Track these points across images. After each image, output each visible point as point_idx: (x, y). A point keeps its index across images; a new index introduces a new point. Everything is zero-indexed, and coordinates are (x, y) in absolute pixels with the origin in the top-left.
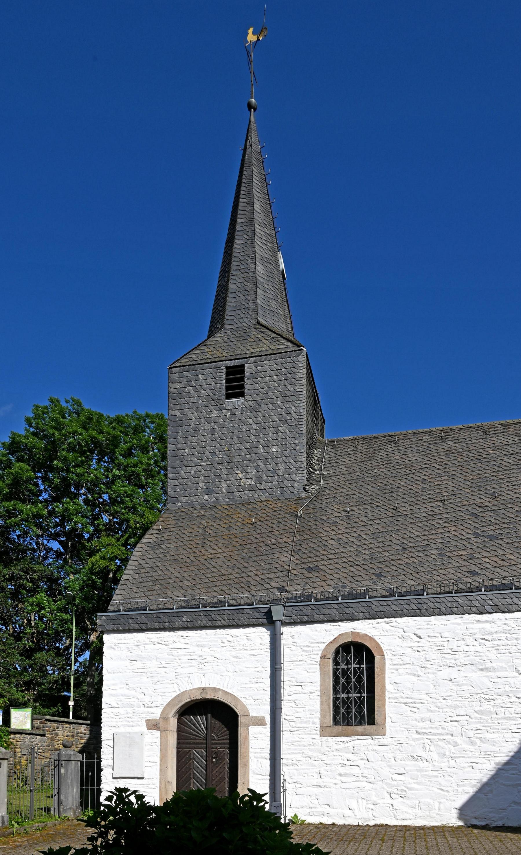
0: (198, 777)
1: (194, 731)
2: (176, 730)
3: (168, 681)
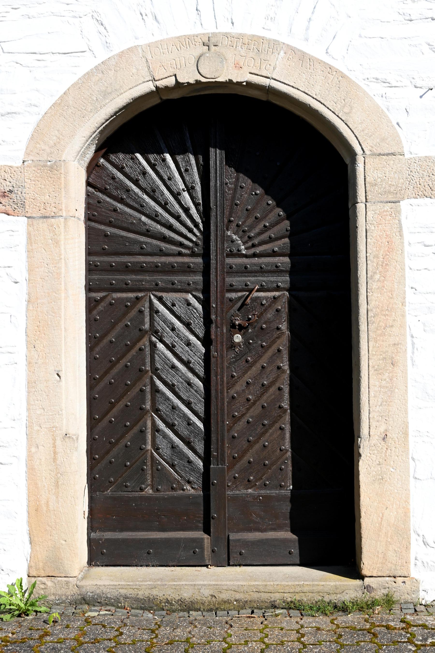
0: (174, 408)
1: (155, 217)
2: (82, 217)
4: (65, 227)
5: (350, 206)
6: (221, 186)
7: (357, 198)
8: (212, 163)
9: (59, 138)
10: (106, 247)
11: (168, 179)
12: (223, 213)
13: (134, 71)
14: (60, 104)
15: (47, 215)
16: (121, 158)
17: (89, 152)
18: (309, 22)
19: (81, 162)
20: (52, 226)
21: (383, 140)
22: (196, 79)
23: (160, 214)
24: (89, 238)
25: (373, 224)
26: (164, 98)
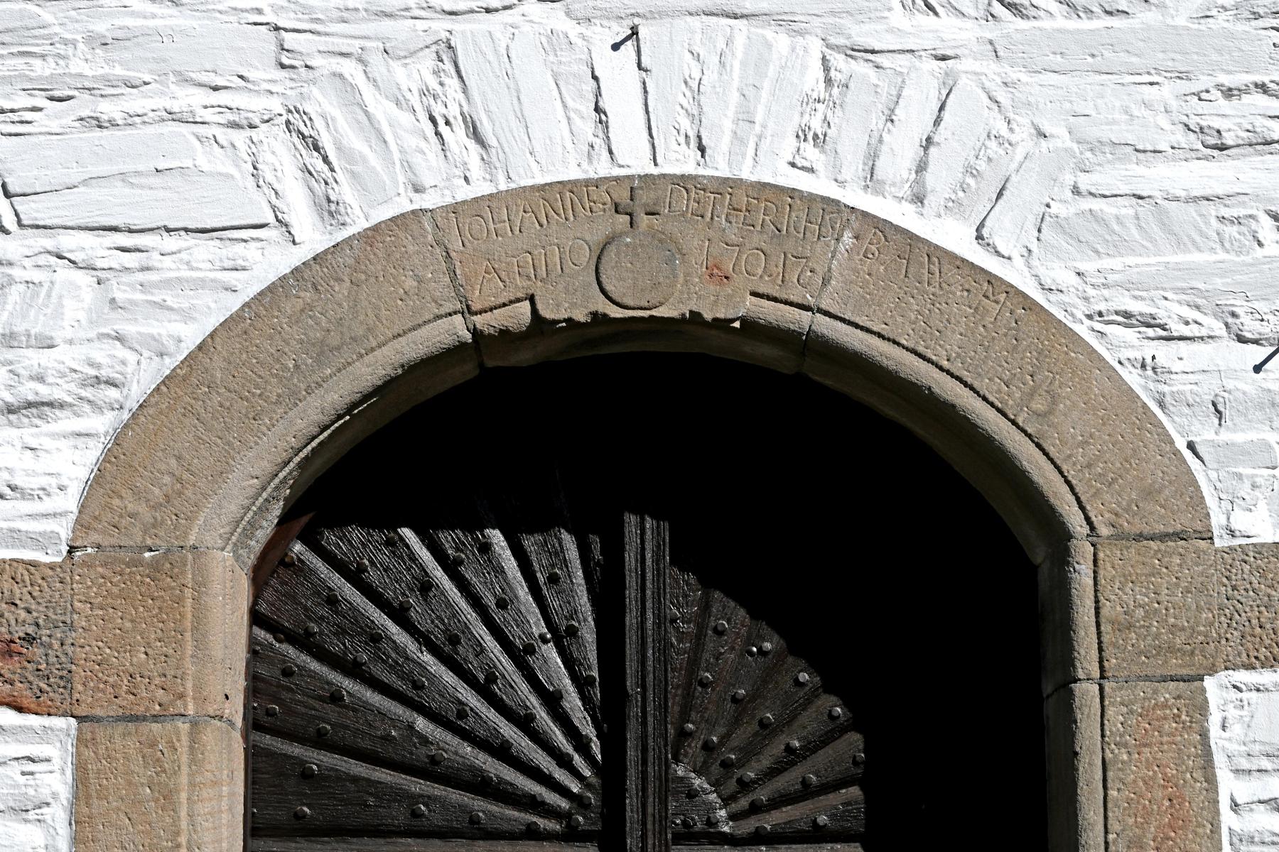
1: (455, 720)
2: (236, 710)
3: (194, 99)
4: (191, 748)
5: (1047, 688)
6: (659, 627)
7: (1074, 667)
8: (630, 558)
9: (180, 480)
10: (306, 809)
11: (498, 605)
12: (663, 708)
13: (410, 283)
14: (187, 380)
15: (140, 710)
16: (355, 542)
17: (265, 524)
18: (926, 149)
19: (241, 551)
20: (153, 745)
21: (1150, 493)
22: (593, 309)
23: (472, 709)
24: (254, 783)
25: (1126, 745)
26: (490, 363)
